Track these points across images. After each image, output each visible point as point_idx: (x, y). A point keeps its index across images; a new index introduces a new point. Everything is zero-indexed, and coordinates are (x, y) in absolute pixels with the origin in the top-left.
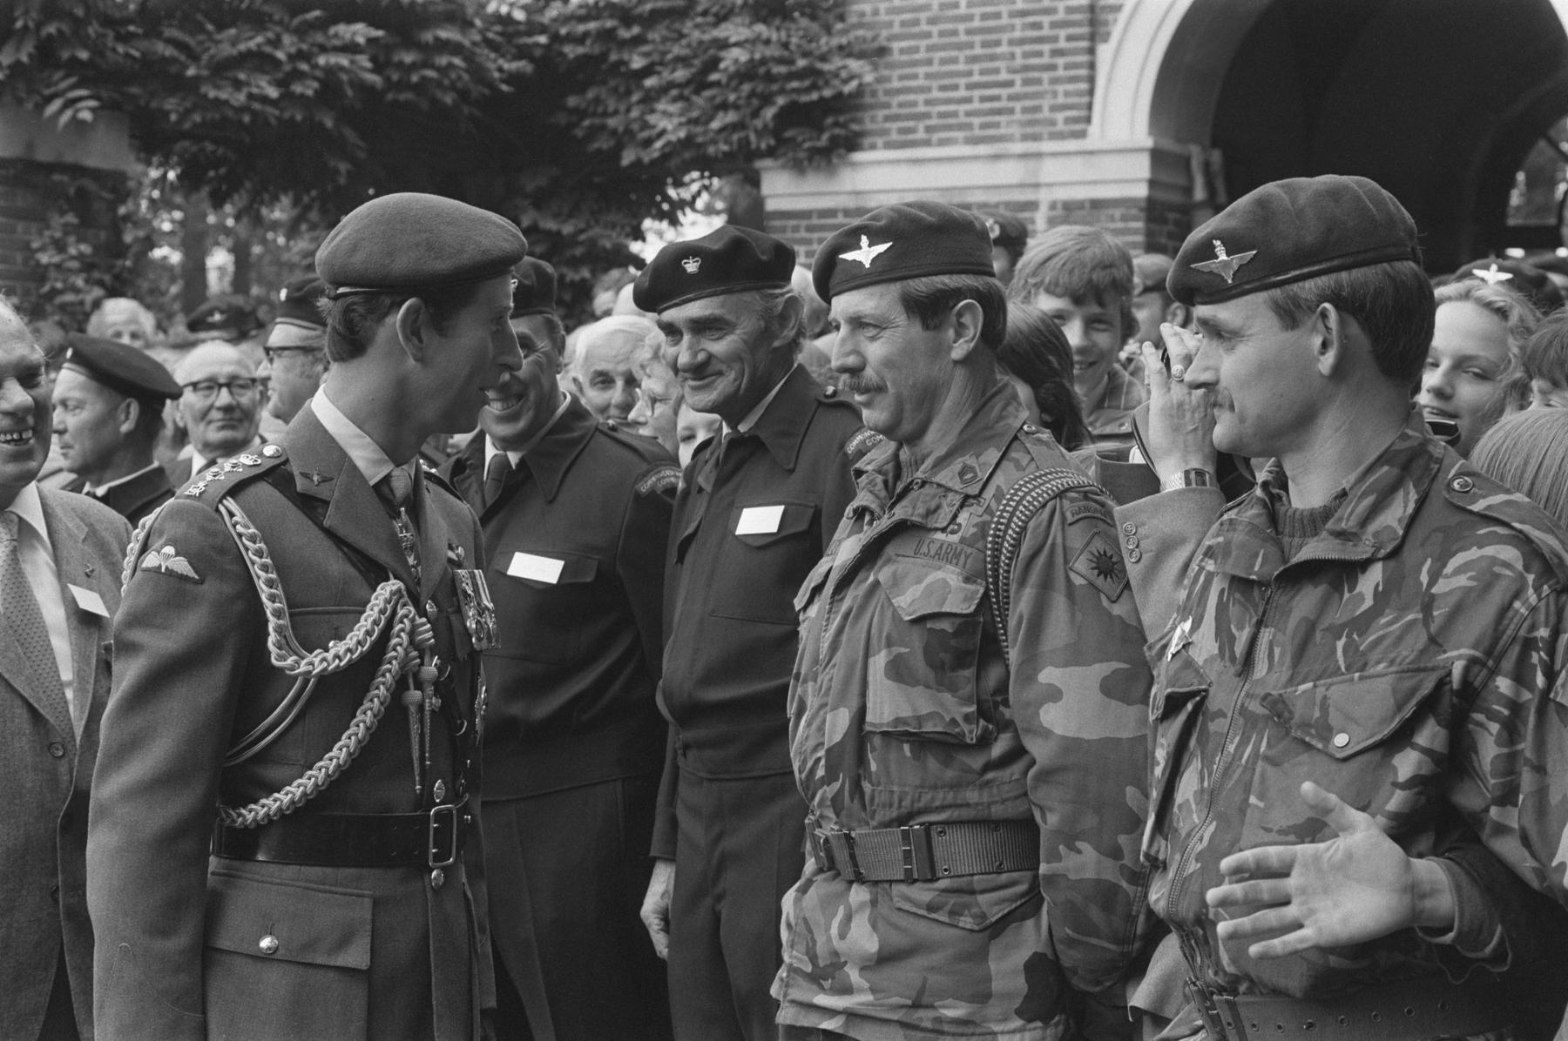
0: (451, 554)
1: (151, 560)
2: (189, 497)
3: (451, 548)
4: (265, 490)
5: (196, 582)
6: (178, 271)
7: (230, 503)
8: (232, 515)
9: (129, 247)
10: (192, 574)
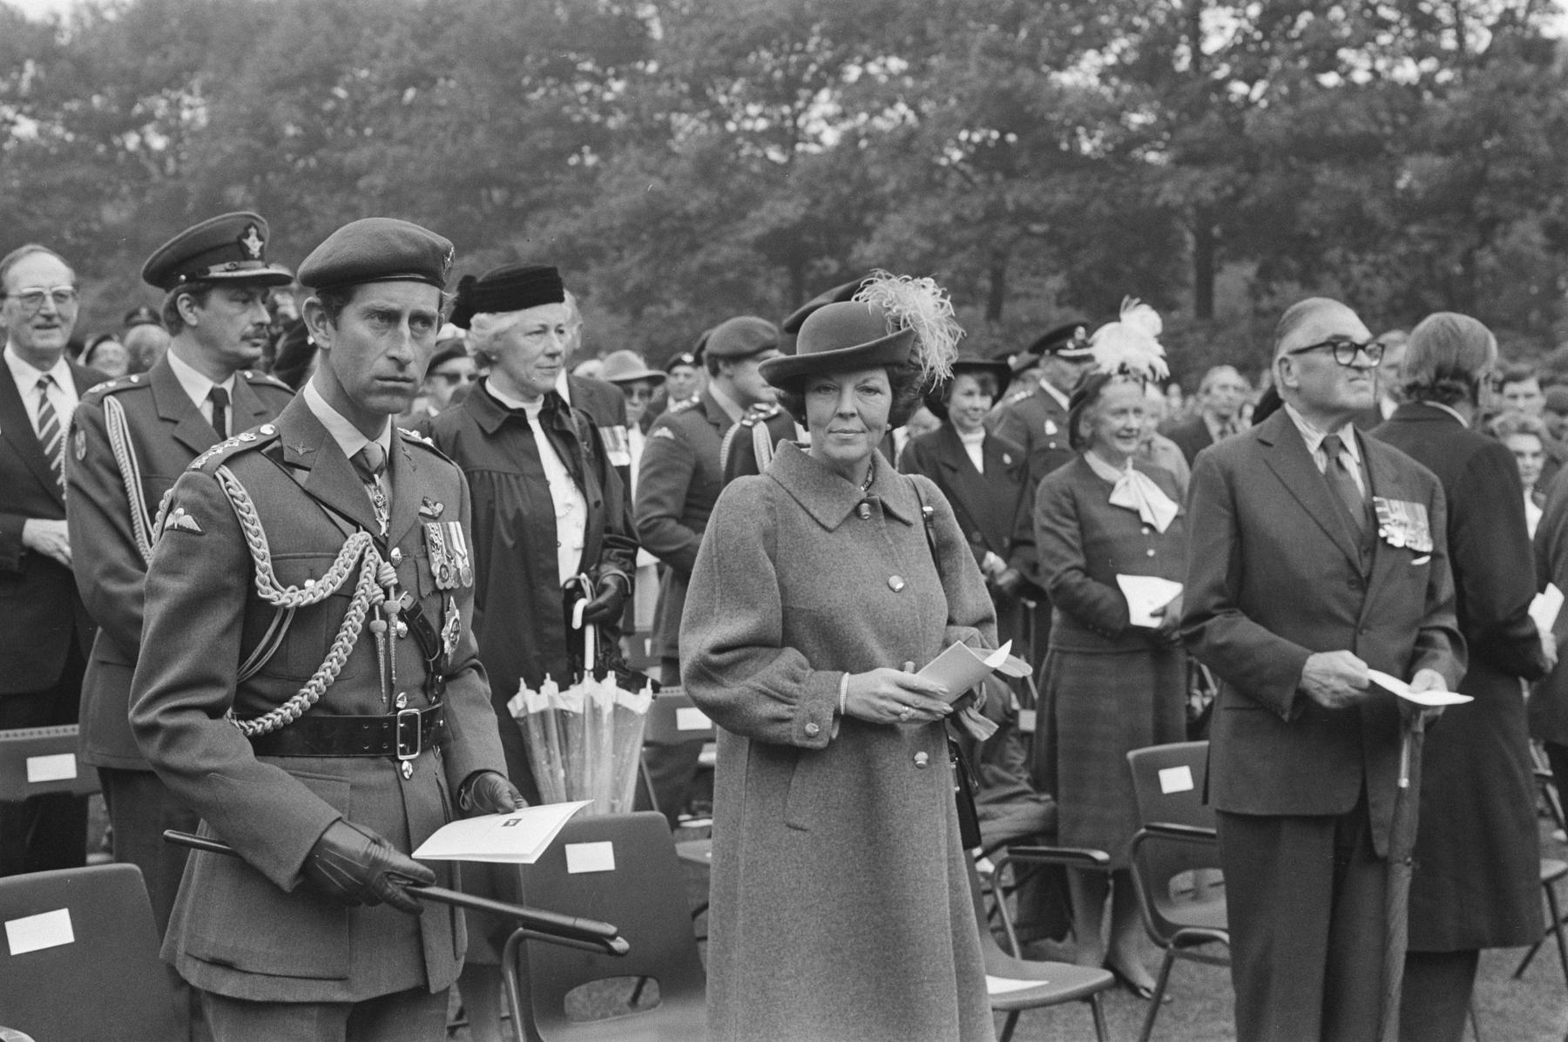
0: (424, 510)
1: (170, 521)
2: (195, 470)
3: (426, 504)
4: (259, 462)
5: (200, 534)
6: (1410, 735)
7: (225, 471)
8: (226, 480)
9: (300, 320)
10: (197, 528)
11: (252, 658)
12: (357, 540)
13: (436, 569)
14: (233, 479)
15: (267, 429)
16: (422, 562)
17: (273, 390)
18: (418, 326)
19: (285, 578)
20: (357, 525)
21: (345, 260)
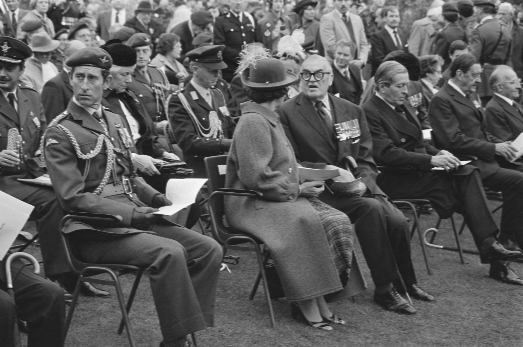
0: (116, 126)
3: (116, 124)
8: (60, 127)
10: (57, 142)
11: (85, 173)
12: (101, 137)
13: (124, 142)
14: (63, 127)
15: (66, 113)
16: (120, 141)
17: (161, 78)
18: (81, 78)
19: (84, 152)
20: (99, 133)
21: (75, 58)
